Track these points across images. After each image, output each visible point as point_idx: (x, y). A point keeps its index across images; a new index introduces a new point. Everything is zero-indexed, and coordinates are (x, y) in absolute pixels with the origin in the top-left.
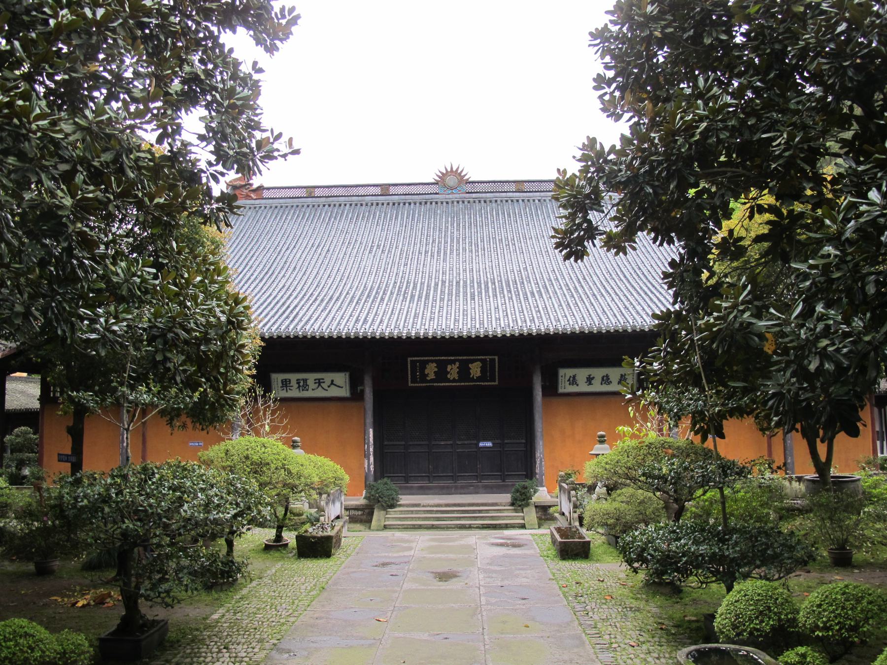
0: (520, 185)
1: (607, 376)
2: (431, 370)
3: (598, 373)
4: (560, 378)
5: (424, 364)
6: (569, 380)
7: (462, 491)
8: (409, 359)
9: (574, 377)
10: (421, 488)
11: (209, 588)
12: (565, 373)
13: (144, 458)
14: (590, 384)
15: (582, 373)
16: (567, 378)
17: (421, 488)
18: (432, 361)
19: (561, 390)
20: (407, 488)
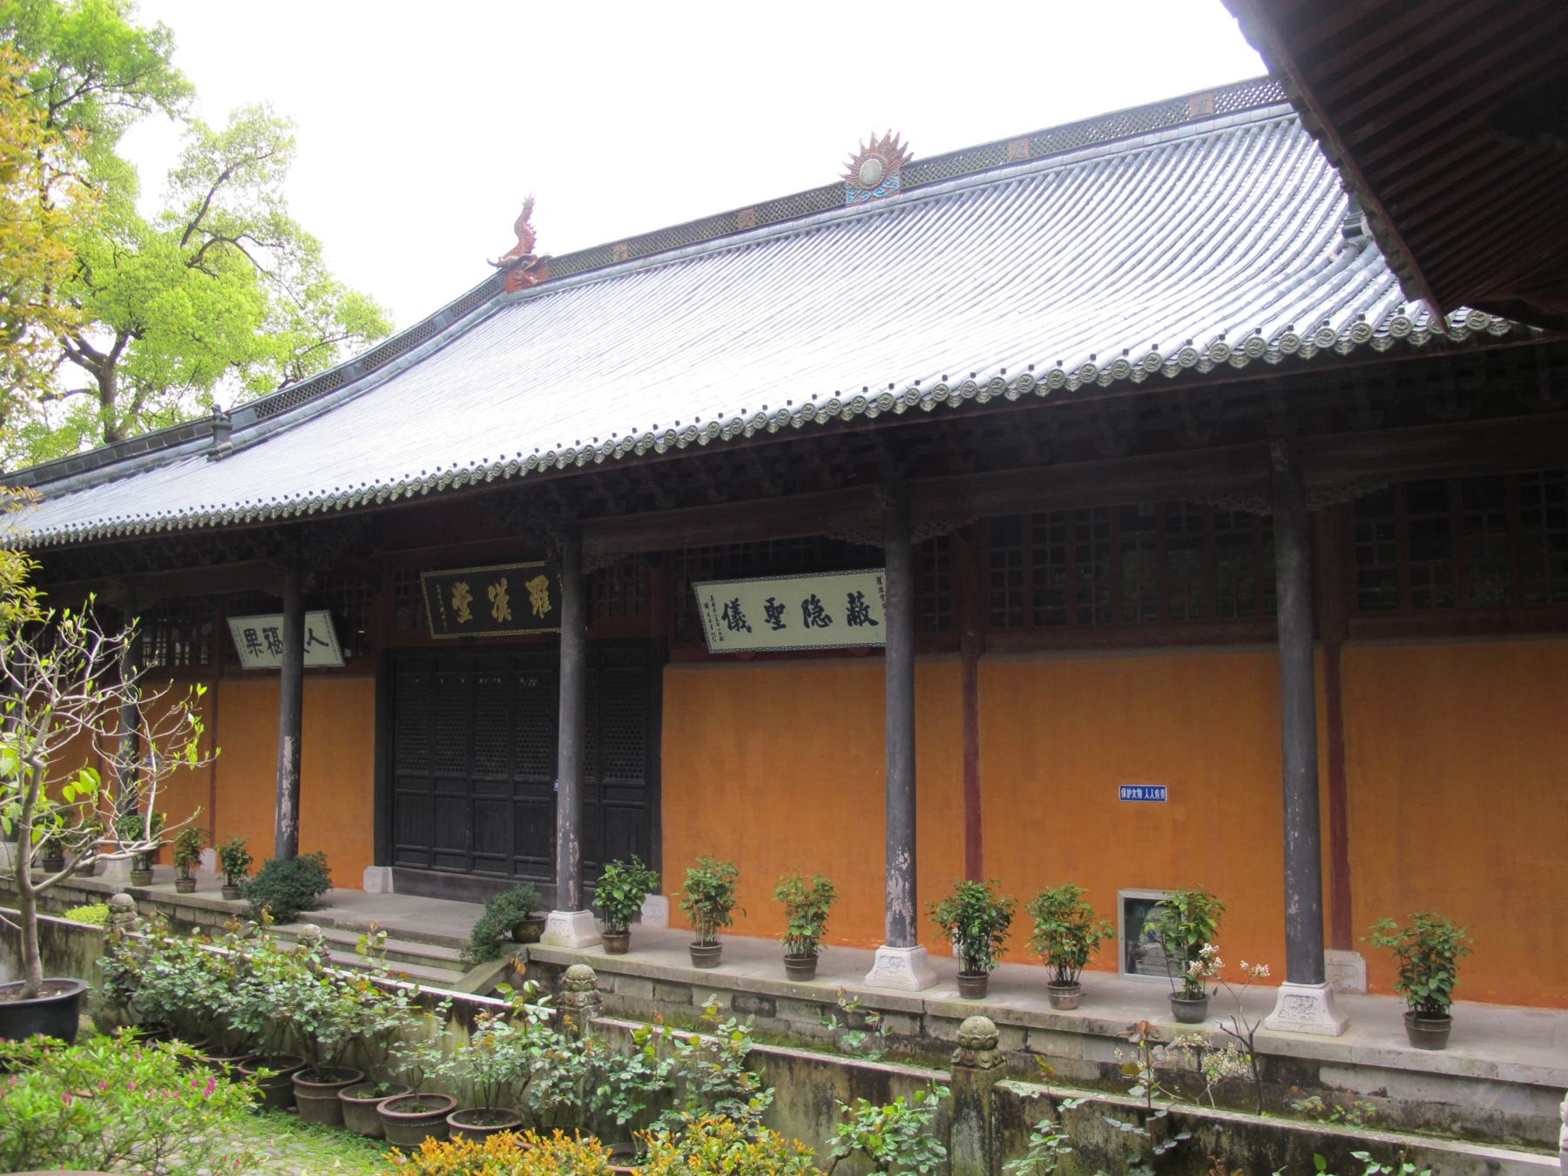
0: (607, 249)
1: (814, 600)
2: (461, 598)
3: (792, 590)
4: (704, 611)
5: (448, 584)
6: (725, 616)
7: (466, 893)
8: (423, 575)
9: (735, 605)
10: (450, 882)
11: (278, 1100)
12: (713, 596)
13: (974, 868)
14: (779, 626)
15: (752, 594)
16: (721, 612)
17: (450, 882)
18: (461, 579)
19: (715, 646)
20: (427, 879)
